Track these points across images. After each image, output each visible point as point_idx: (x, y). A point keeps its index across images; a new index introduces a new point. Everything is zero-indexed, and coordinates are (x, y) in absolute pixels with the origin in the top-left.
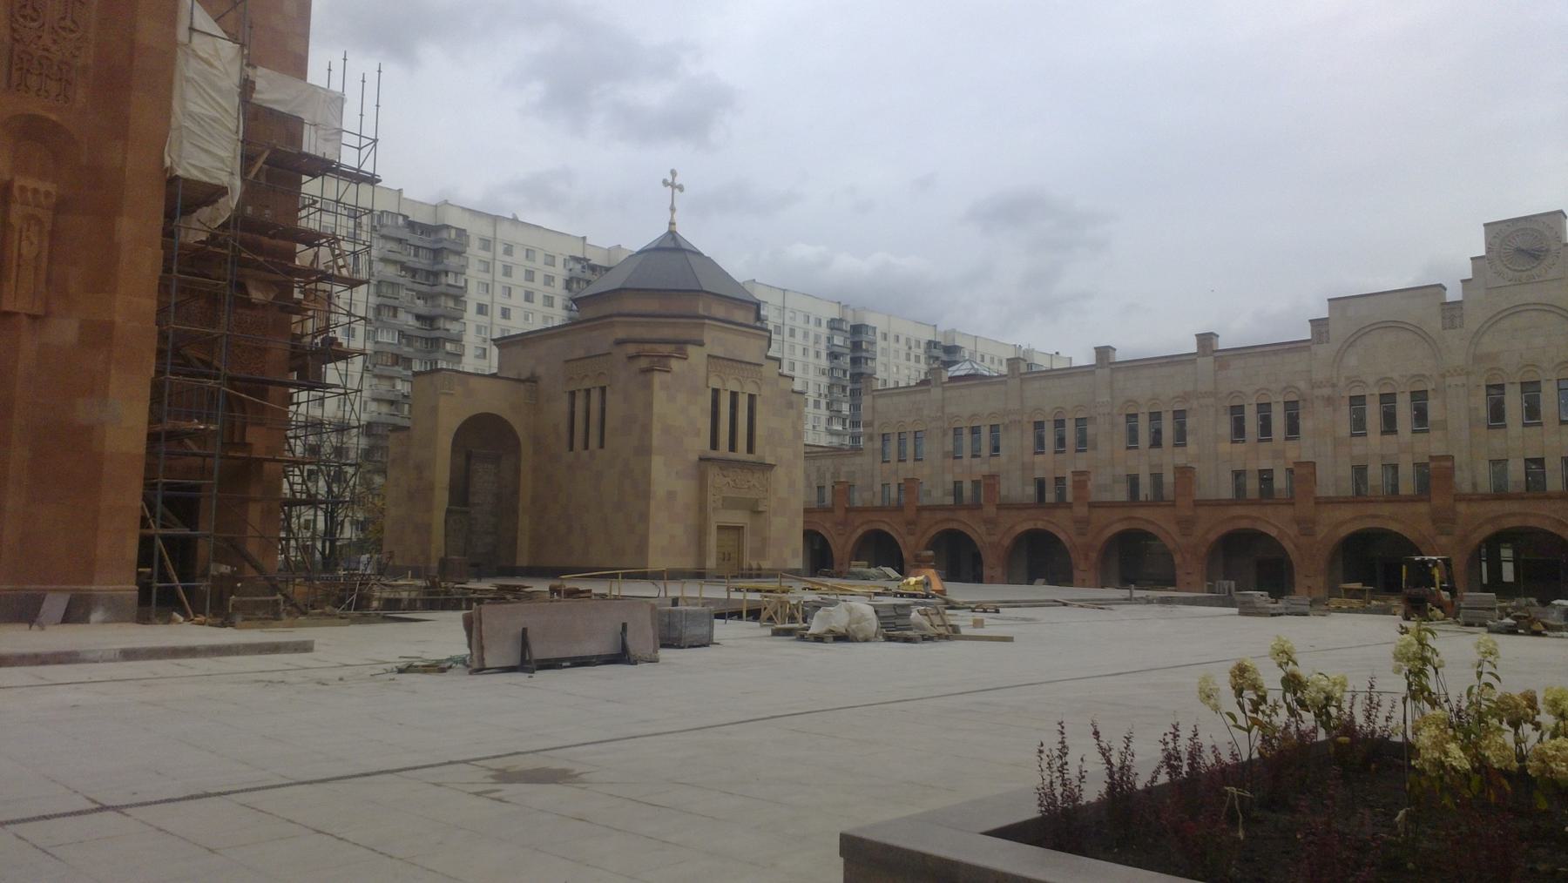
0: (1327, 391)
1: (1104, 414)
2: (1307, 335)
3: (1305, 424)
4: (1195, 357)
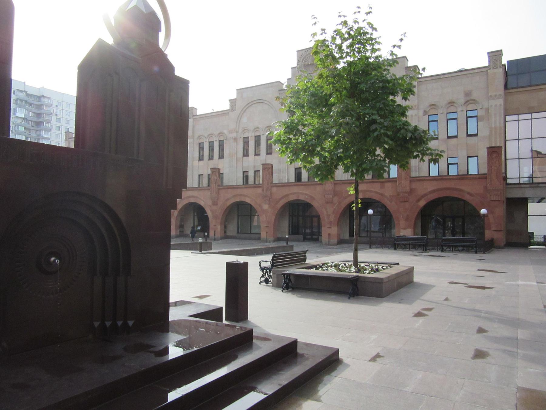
0: (234, 135)
2: (542, 240)
3: (226, 152)
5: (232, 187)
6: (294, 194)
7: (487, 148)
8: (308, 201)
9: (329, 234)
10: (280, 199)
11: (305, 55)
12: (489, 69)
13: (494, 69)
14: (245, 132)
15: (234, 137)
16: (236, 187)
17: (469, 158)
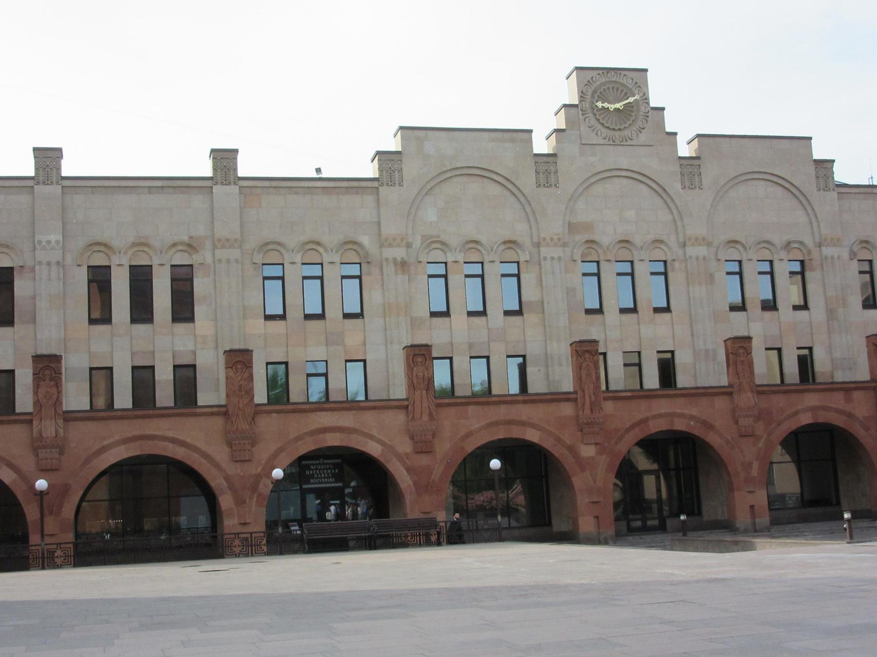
0: (399, 253)
1: (49, 264)
2: (370, 171)
4: (30, 183)
5: (563, 396)
6: (661, 416)
7: (33, 357)
8: (696, 432)
9: (752, 507)
10: (628, 430)
11: (598, 83)
12: (36, 183)
13: (546, 188)
14: (736, 248)
15: (399, 259)
16: (694, 391)
17: (485, 360)
